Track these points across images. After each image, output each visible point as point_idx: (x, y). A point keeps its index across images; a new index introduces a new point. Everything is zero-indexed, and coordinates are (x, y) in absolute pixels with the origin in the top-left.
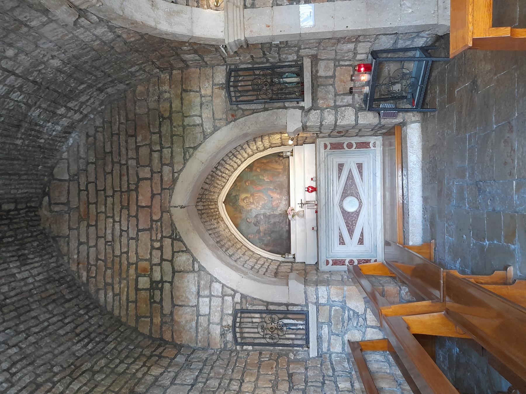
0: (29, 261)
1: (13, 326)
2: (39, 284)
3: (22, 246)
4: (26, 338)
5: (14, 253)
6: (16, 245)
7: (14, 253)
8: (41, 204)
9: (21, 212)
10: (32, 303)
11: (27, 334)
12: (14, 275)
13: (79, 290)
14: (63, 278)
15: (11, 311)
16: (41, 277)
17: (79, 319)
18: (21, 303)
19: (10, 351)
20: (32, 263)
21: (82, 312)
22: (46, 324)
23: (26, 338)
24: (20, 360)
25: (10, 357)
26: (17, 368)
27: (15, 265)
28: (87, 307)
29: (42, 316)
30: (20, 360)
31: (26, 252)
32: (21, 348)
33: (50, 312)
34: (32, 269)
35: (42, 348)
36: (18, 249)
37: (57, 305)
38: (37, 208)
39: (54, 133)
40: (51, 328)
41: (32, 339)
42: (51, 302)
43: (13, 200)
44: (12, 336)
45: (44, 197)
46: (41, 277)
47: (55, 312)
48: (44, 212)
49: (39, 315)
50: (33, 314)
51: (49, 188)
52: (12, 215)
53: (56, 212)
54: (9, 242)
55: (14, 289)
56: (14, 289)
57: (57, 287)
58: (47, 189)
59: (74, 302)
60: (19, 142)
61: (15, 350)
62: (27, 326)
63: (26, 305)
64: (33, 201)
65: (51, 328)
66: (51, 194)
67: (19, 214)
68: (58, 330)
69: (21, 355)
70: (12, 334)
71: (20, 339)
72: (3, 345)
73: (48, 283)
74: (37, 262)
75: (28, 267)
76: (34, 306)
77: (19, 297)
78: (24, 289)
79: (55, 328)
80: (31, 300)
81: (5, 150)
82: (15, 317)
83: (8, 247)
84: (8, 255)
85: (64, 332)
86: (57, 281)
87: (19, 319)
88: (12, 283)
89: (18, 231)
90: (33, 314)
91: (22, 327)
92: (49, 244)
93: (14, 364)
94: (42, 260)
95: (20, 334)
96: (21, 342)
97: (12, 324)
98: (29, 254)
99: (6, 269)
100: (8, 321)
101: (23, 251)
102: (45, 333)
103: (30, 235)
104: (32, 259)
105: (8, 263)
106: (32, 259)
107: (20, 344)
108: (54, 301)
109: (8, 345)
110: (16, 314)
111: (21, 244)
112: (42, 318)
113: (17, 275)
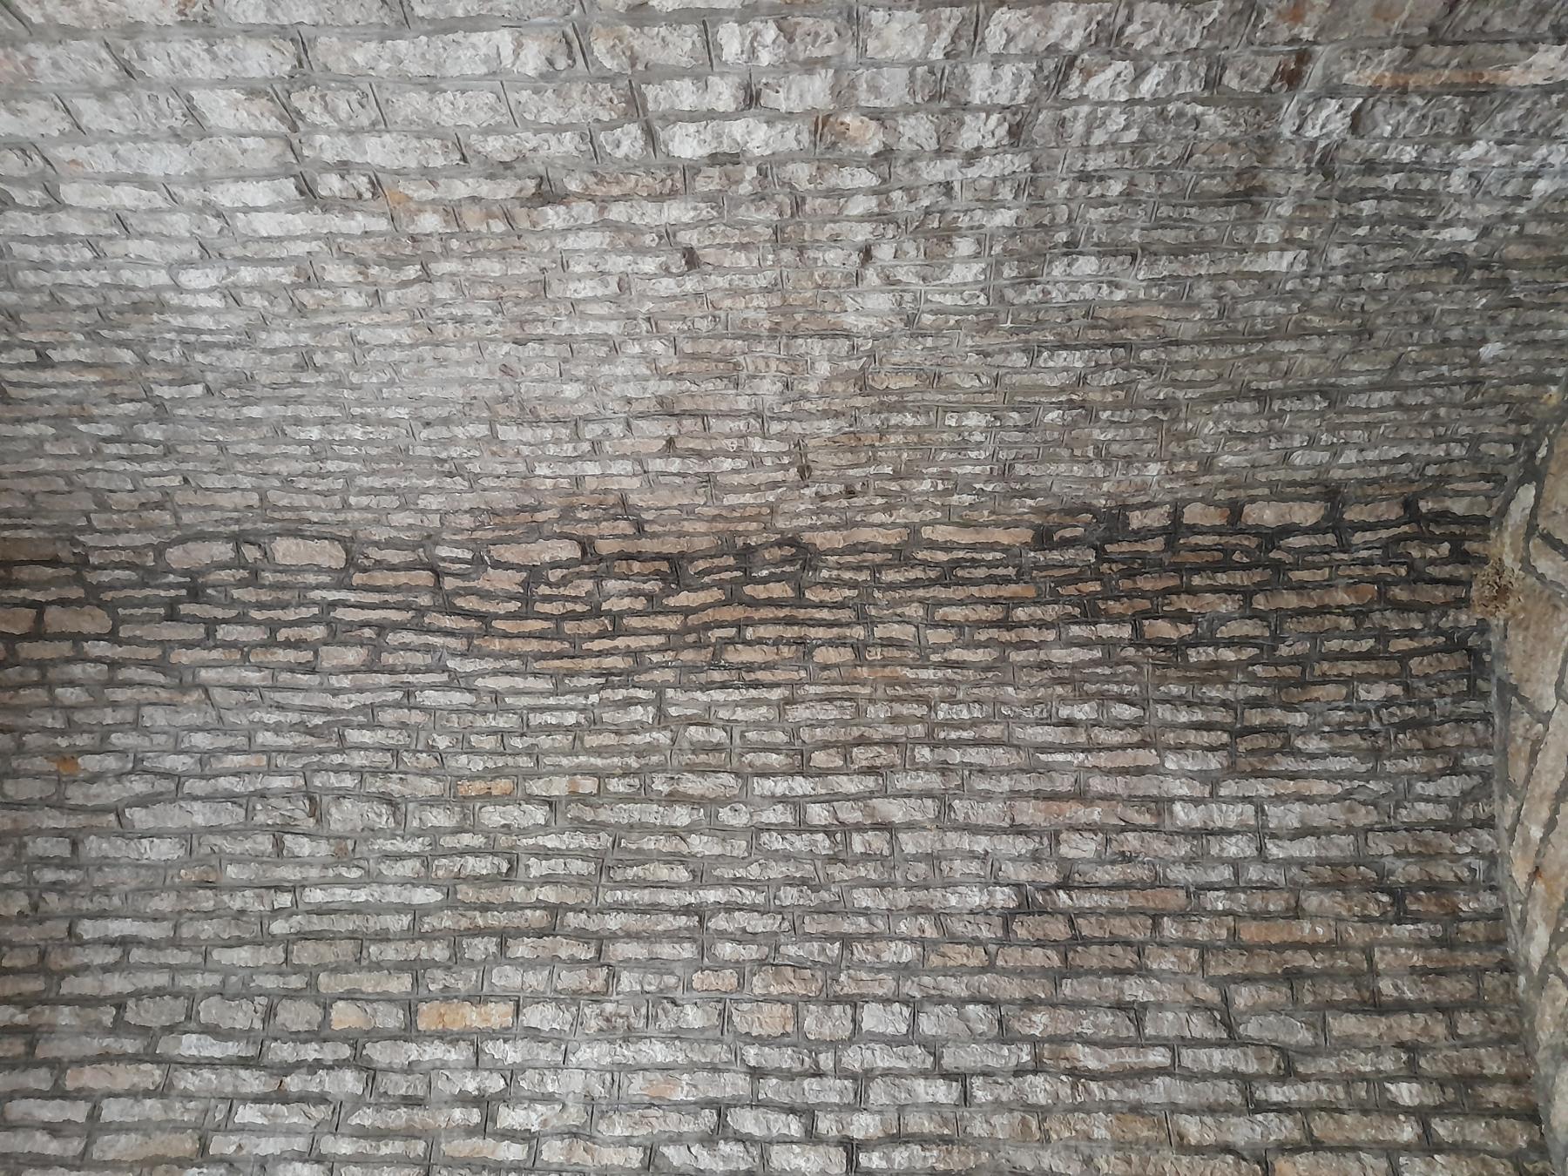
0: (1287, 764)
1: (1012, 1002)
2: (1271, 875)
3: (1295, 683)
4: (1019, 1072)
5: (1219, 716)
6: (1255, 681)
7: (1219, 716)
8: (1503, 512)
9: (1358, 538)
10: (1162, 945)
11: (1037, 1058)
12: (1161, 804)
13: (1491, 981)
14: (1434, 887)
15: (1040, 944)
16: (1305, 849)
17: (1348, 1119)
18: (1120, 926)
19: (920, 1085)
20: (1293, 776)
21: (1405, 1093)
22: (1158, 1057)
23: (1019, 1072)
24: (924, 1140)
25: (901, 1109)
26: (889, 1160)
27: (1189, 765)
28: (1468, 1081)
29: (1170, 1016)
30: (924, 1140)
31: (1299, 719)
32: (966, 1098)
33: (1226, 1017)
34: (1279, 799)
35: (1046, 1140)
36: (1257, 703)
37: (1295, 1001)
38: (1484, 521)
39: (1541, 187)
40: (1160, 1091)
41: (1039, 1089)
42: (1271, 979)
43: (1312, 490)
44: (975, 1037)
45: (1520, 482)
46: (1305, 849)
47: (1251, 1029)
48: (1505, 548)
49: (1160, 1006)
50: (1135, 990)
51: (1550, 448)
52: (1289, 550)
53: (1541, 577)
54: (1216, 665)
55: (1126, 858)
56: (1126, 858)
57: (1366, 919)
58: (1542, 452)
59: (1406, 1027)
60: (1279, 263)
61: (943, 1092)
62: (1062, 1030)
63: (1127, 943)
64: (1459, 494)
65: (1160, 1091)
66: (1549, 482)
67: (1344, 547)
68: (1191, 1111)
69: (945, 1122)
70: (982, 1028)
71: (992, 1062)
72: (918, 1050)
73: (1323, 886)
74: (1333, 777)
75: (1260, 788)
76: (1164, 962)
77: (1123, 900)
78: (1178, 873)
79: (1181, 1099)
80: (1170, 929)
81: (1195, 305)
82: (1044, 971)
83: (1204, 682)
84: (1183, 717)
85: (1210, 1138)
86: (1389, 891)
87: (1057, 986)
88: (1130, 836)
89: (1290, 625)
90: (1135, 990)
91: (1039, 1023)
92: (1474, 706)
93: (899, 1138)
94: (1372, 775)
95: (1012, 1042)
96: (986, 1073)
97: (1013, 989)
98: (1303, 732)
99: (1140, 771)
100: (1004, 972)
101: (1278, 715)
102: (1113, 1094)
103: (1366, 645)
104: (1312, 757)
105: (1163, 749)
106: (1312, 757)
107: (978, 1081)
108: (1292, 977)
109: (937, 1058)
110: (1056, 961)
111: (1282, 683)
112: (1166, 1024)
113: (1177, 807)
